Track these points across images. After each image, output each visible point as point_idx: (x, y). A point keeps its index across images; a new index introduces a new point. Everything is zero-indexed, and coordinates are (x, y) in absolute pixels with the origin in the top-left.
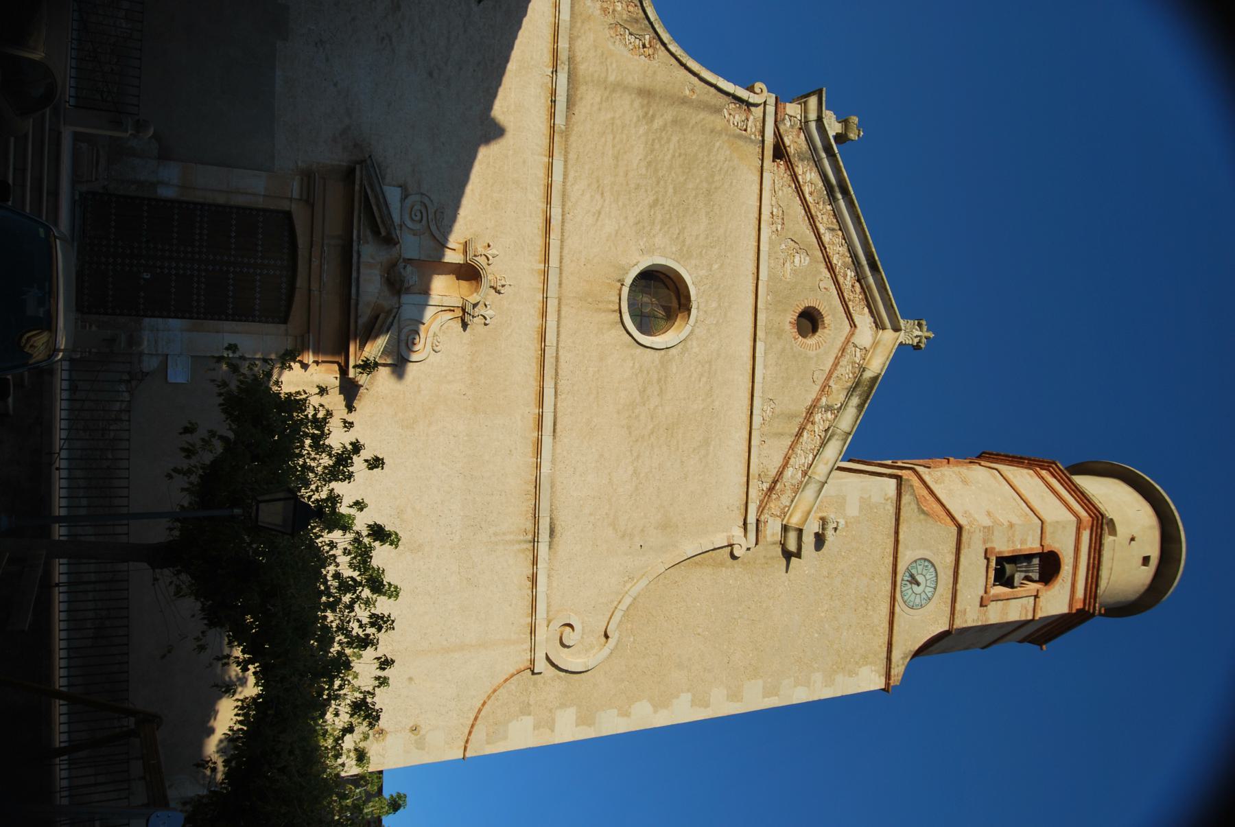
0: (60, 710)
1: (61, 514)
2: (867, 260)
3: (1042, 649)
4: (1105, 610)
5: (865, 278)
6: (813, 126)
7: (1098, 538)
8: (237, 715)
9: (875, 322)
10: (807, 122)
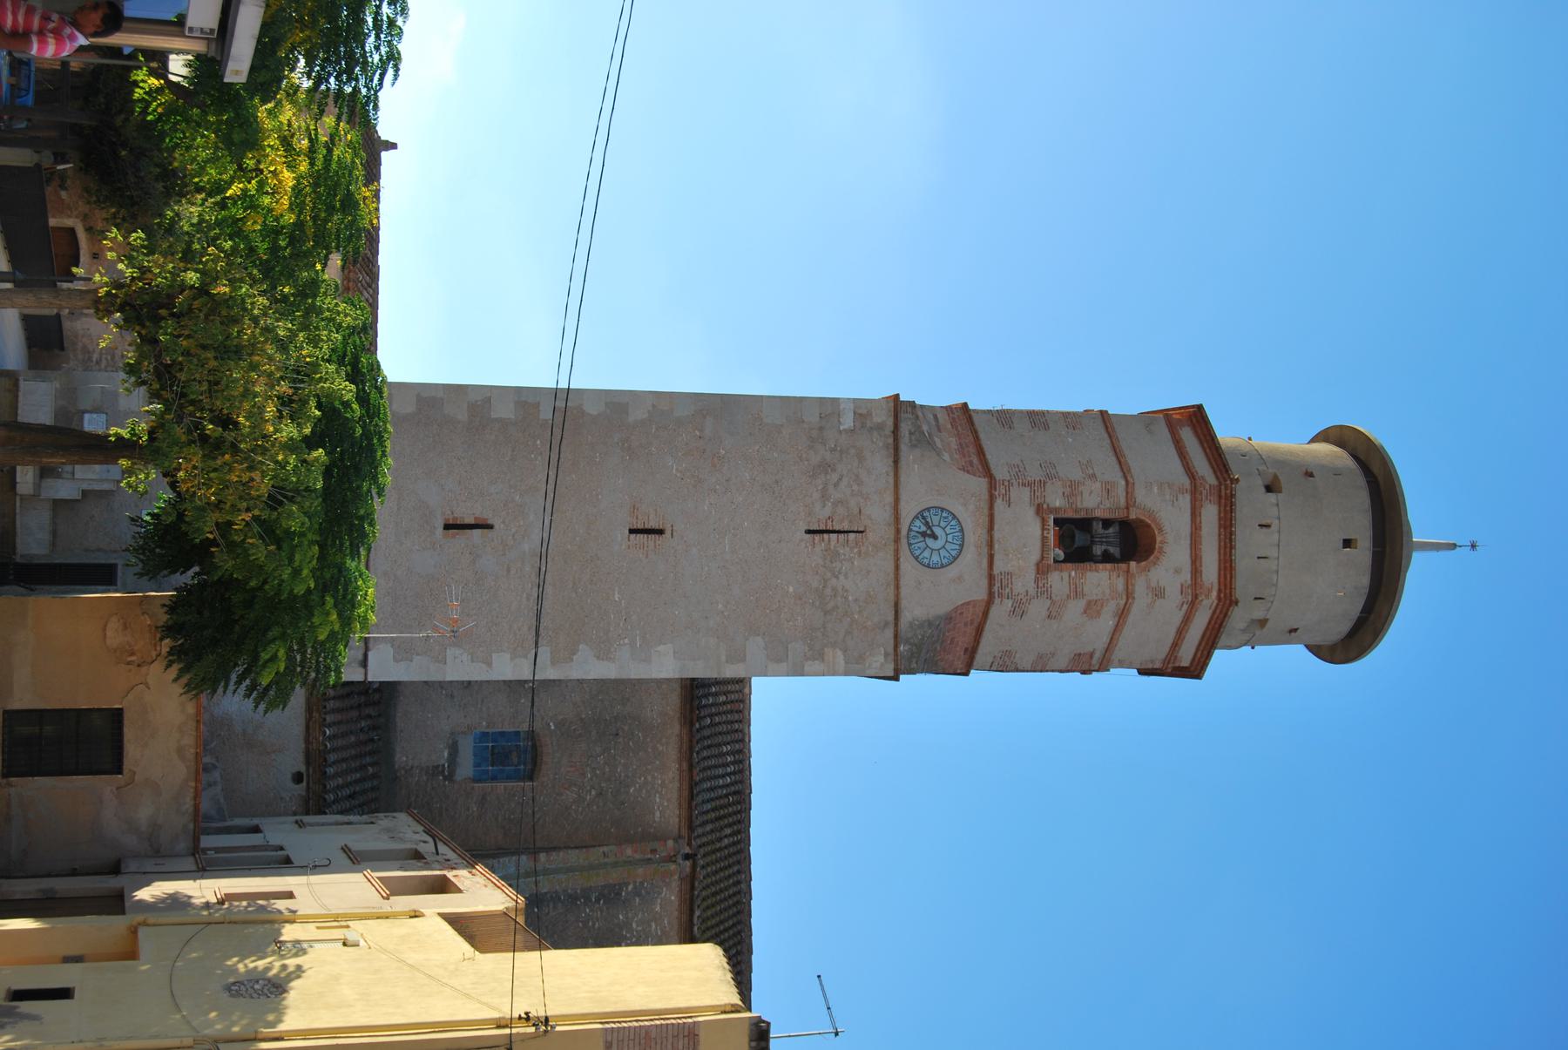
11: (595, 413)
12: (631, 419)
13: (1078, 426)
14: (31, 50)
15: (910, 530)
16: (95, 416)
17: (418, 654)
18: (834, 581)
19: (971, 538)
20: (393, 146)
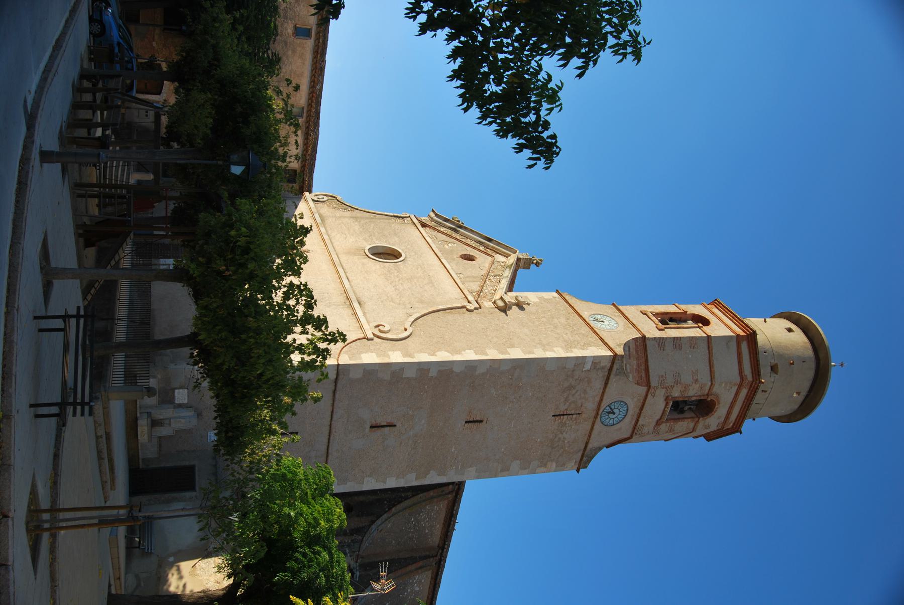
0: (107, 180)
1: (60, 507)
2: (486, 240)
3: (763, 383)
4: (108, 148)
5: (489, 245)
6: (435, 218)
7: (723, 307)
8: (83, 414)
9: (505, 256)
10: (432, 218)
11: (459, 371)
12: (477, 373)
13: (696, 346)
15: (603, 411)
16: (181, 390)
18: (560, 435)
19: (631, 412)
20: (741, 433)
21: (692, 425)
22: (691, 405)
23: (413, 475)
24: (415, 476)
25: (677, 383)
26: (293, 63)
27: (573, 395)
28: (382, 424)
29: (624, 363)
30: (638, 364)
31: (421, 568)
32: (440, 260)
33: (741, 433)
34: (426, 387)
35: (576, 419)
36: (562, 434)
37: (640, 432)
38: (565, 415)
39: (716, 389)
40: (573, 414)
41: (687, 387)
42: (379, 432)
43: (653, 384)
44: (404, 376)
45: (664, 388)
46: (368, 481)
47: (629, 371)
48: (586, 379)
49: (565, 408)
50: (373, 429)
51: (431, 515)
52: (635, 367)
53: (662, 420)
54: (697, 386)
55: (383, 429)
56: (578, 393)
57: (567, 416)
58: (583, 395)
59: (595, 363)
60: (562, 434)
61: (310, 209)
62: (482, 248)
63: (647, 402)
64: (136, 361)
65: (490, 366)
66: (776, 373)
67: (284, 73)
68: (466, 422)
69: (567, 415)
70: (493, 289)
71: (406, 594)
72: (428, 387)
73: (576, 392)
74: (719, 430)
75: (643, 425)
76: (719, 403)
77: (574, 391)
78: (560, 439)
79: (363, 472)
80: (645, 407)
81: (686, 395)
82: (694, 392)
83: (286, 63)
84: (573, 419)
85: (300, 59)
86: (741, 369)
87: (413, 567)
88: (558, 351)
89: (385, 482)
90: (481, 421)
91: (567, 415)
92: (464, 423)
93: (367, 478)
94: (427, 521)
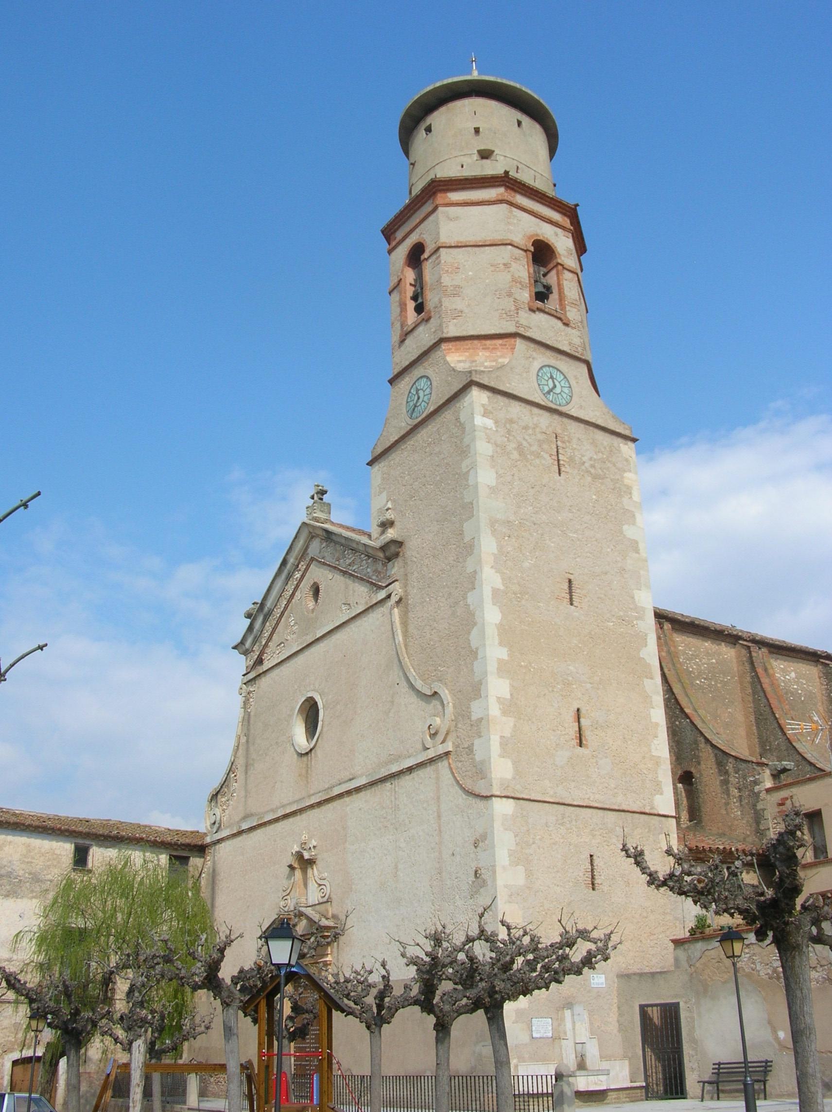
11: (500, 615)
12: (502, 587)
13: (456, 265)
14: (221, 1108)
15: (552, 402)
16: (534, 1028)
17: (657, 777)
18: (587, 465)
19: (552, 362)
20: (577, 205)
21: (567, 275)
22: (539, 273)
23: (647, 682)
24: (649, 680)
25: (510, 295)
26: (10, 859)
27: (530, 445)
28: (577, 729)
29: (482, 369)
30: (483, 349)
31: (766, 670)
32: (318, 640)
33: (577, 205)
34: (523, 663)
35: (563, 442)
36: (584, 462)
37: (579, 349)
38: (558, 457)
39: (518, 239)
40: (557, 447)
41: (514, 280)
42: (587, 734)
43: (512, 329)
44: (508, 697)
45: (517, 313)
46: (656, 749)
47: (494, 364)
48: (508, 426)
49: (549, 458)
50: (584, 742)
51: (692, 655)
52: (487, 354)
53: (562, 317)
54: (514, 266)
55: (583, 728)
56: (527, 437)
57: (560, 455)
58: (530, 431)
59: (485, 413)
60: (584, 462)
61: (234, 836)
62: (298, 575)
63: (538, 338)
64: (490, 1095)
65: (492, 567)
66: (492, 152)
67: (25, 873)
68: (572, 604)
69: (558, 455)
70: (366, 560)
71: (800, 692)
72: (523, 661)
73: (526, 440)
74: (573, 236)
75: (570, 344)
76: (537, 235)
77: (525, 444)
78: (593, 466)
79: (644, 758)
80: (544, 341)
81: (528, 282)
82: (523, 269)
83: (10, 870)
84: (564, 446)
85: (5, 849)
86: (488, 201)
87: (765, 681)
88: (467, 466)
89: (657, 724)
90: (570, 581)
91: (558, 455)
92: (572, 607)
93: (653, 751)
94: (701, 661)
